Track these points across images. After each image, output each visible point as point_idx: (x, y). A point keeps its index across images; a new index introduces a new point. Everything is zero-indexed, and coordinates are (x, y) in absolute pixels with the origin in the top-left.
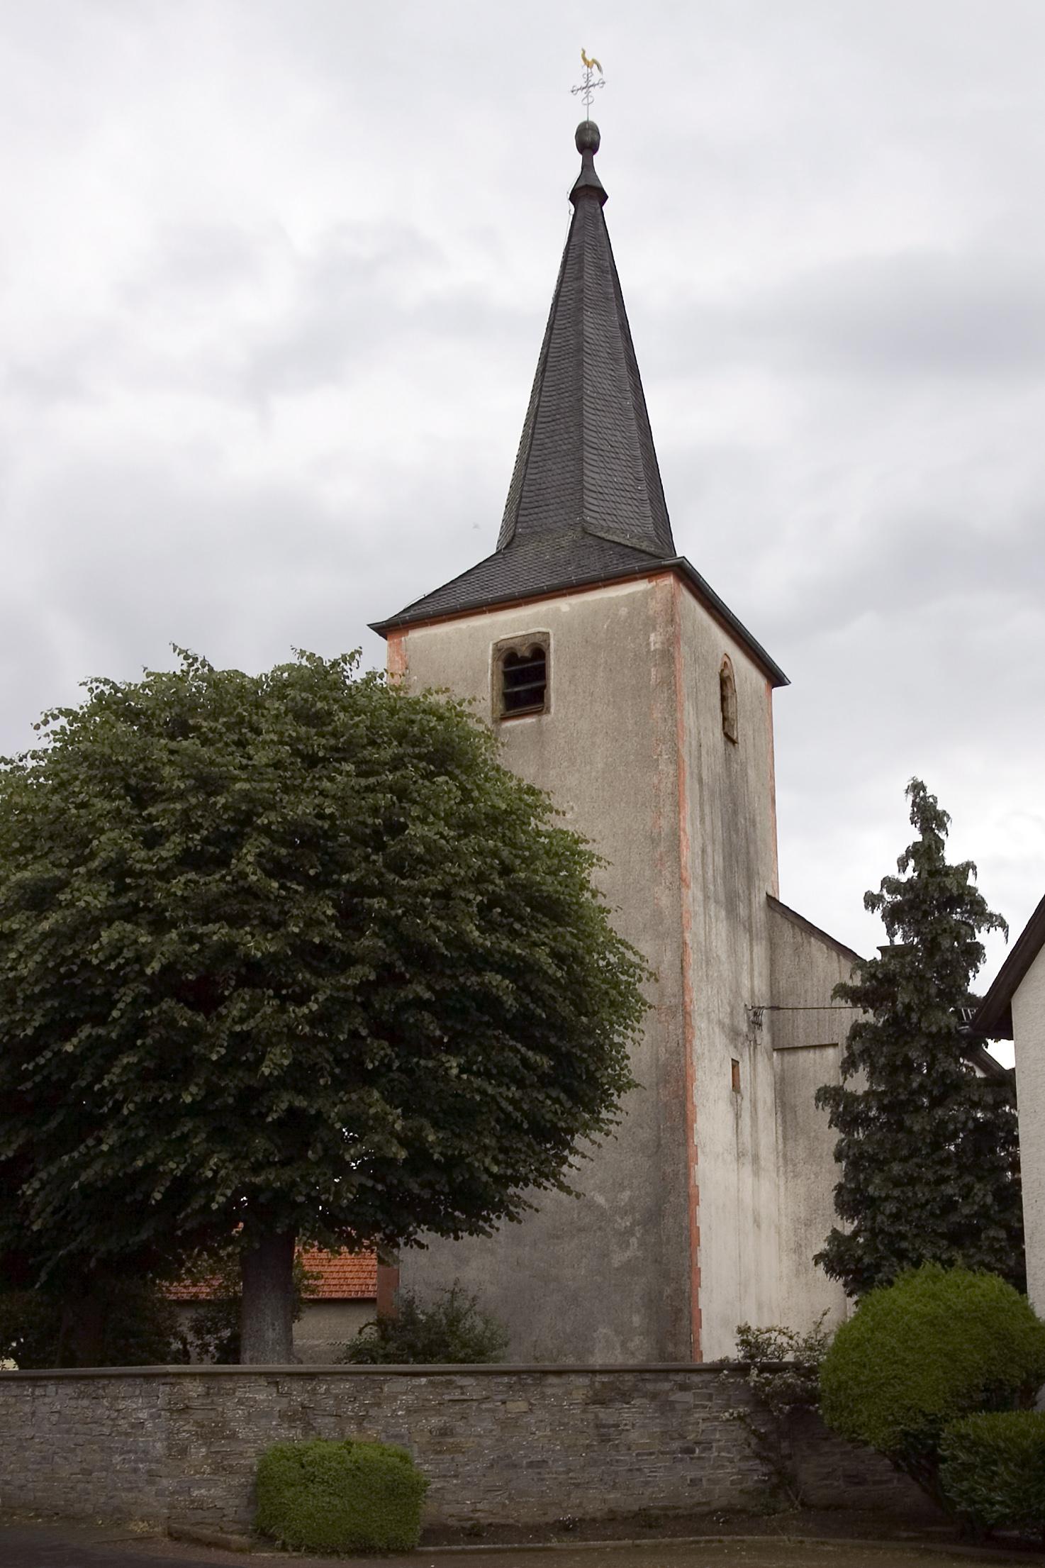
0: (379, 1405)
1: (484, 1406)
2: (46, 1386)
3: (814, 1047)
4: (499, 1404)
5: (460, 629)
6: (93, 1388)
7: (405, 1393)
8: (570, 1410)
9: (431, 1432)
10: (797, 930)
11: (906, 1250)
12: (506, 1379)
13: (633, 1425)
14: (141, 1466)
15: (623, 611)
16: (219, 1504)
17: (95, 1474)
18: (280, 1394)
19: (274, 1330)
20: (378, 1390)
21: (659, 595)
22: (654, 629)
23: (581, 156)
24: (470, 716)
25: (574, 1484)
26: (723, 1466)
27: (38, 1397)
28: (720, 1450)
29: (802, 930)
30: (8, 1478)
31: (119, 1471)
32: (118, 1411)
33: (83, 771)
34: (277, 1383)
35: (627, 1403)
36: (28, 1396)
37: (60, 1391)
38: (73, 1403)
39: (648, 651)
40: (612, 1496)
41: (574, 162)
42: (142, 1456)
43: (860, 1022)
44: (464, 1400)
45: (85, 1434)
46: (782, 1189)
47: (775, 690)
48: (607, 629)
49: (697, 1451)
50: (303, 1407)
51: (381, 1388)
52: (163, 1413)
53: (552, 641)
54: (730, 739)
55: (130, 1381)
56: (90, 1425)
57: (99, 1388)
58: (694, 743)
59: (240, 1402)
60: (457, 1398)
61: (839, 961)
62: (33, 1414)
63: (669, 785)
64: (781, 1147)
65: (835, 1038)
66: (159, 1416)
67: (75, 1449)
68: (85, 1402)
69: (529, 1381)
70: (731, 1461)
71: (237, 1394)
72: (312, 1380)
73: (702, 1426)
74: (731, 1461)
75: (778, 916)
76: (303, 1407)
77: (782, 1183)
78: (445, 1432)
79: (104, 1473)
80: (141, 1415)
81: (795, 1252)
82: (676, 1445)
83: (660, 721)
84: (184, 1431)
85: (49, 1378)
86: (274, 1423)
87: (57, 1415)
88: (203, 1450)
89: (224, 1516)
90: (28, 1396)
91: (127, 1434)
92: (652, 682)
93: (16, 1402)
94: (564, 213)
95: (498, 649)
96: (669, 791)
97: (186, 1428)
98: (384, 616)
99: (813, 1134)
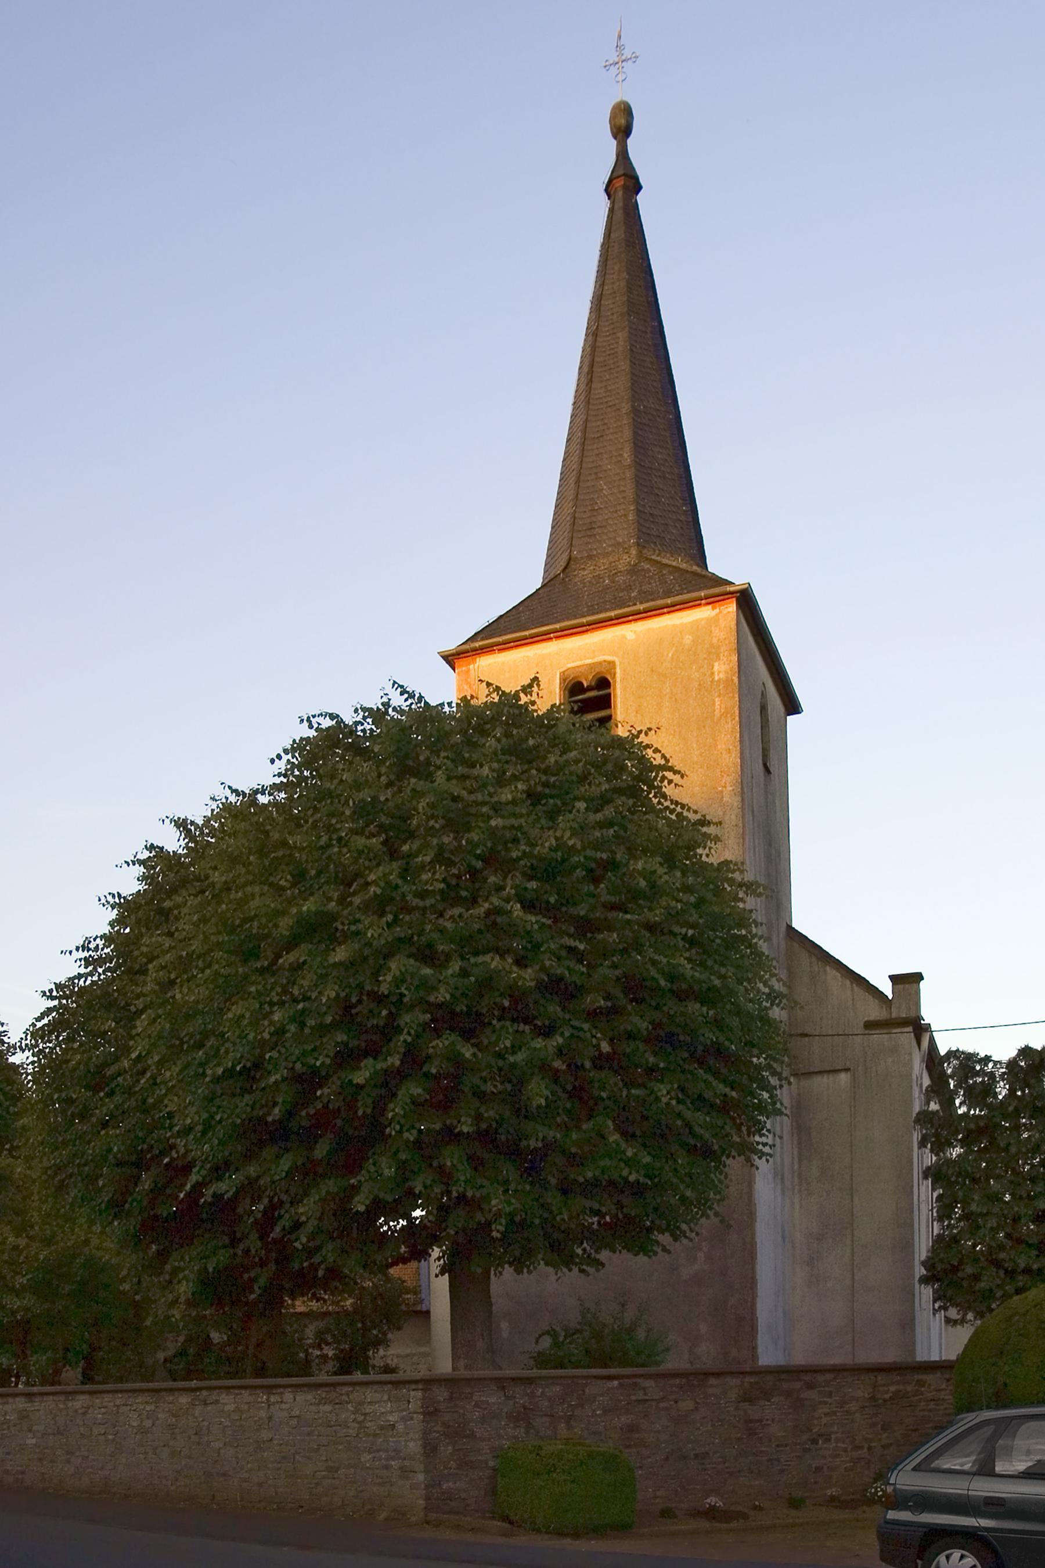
0: (582, 1406)
1: (662, 1405)
2: (282, 1393)
3: (829, 1072)
4: (672, 1403)
5: (528, 657)
6: (335, 1394)
7: (602, 1395)
8: (726, 1407)
9: (621, 1429)
10: (814, 959)
11: (1004, 1260)
12: (677, 1381)
13: (773, 1420)
14: (393, 1463)
15: (688, 640)
16: (463, 1495)
17: (342, 1471)
18: (507, 1398)
19: (483, 1339)
20: (581, 1392)
21: (722, 623)
22: (718, 658)
23: (615, 142)
24: (648, 746)
25: (728, 1472)
26: (838, 1456)
27: (274, 1404)
28: (837, 1441)
29: (818, 959)
30: (246, 1475)
31: (367, 1468)
32: (365, 1414)
33: (224, 800)
34: (504, 1387)
35: (769, 1401)
36: (263, 1402)
37: (298, 1398)
38: (313, 1408)
39: (712, 681)
40: (757, 1483)
41: (611, 145)
42: (393, 1454)
43: (952, 1049)
44: (647, 1400)
45: (327, 1436)
46: (797, 1207)
47: (788, 717)
48: (672, 658)
49: (820, 1442)
50: (525, 1408)
51: (584, 1391)
52: (415, 1416)
53: (618, 671)
54: (767, 770)
55: (376, 1387)
56: (334, 1428)
57: (342, 1395)
58: (750, 775)
59: (477, 1405)
60: (640, 1398)
61: (852, 990)
62: (270, 1418)
63: (733, 817)
64: (796, 1167)
65: (848, 1063)
66: (412, 1419)
67: (318, 1449)
68: (328, 1408)
69: (695, 1382)
70: (845, 1450)
71: (474, 1398)
72: (531, 1384)
73: (824, 1420)
74: (845, 1450)
75: (796, 945)
76: (525, 1409)
77: (796, 1200)
78: (632, 1428)
79: (352, 1470)
80: (391, 1418)
81: (808, 1265)
82: (805, 1437)
83: (724, 752)
84: (435, 1431)
85: (286, 1386)
86: (503, 1423)
87: (296, 1420)
88: (450, 1448)
89: (468, 1505)
90: (263, 1402)
91: (375, 1435)
92: (717, 712)
93: (249, 1408)
94: (602, 205)
95: (563, 679)
96: (734, 823)
97: (435, 1429)
98: (452, 644)
99: (825, 1155)
